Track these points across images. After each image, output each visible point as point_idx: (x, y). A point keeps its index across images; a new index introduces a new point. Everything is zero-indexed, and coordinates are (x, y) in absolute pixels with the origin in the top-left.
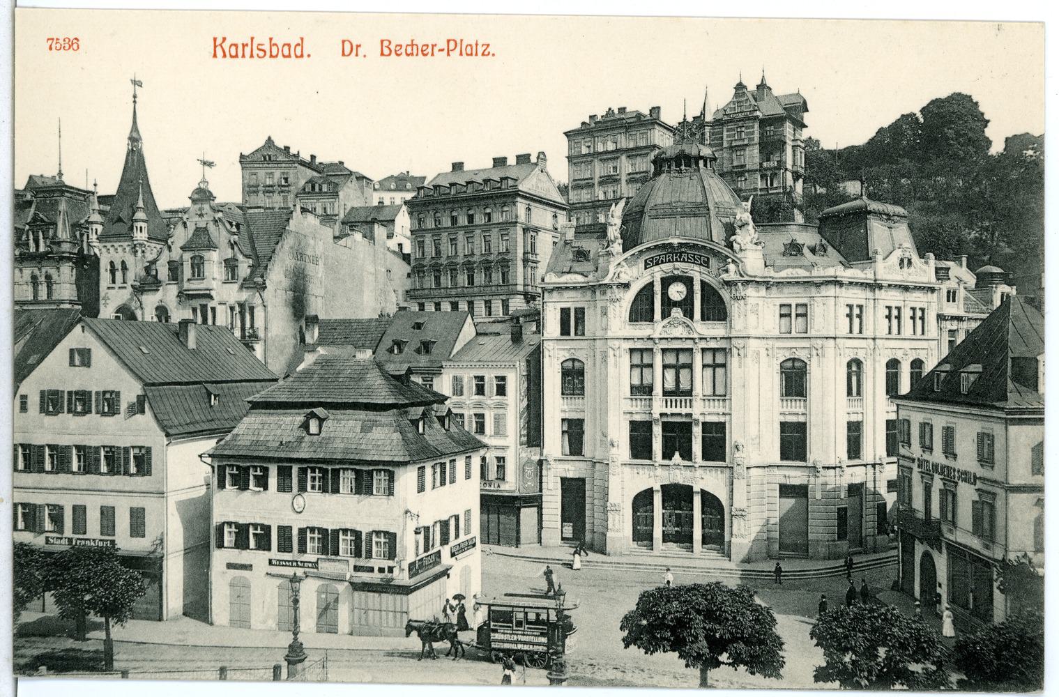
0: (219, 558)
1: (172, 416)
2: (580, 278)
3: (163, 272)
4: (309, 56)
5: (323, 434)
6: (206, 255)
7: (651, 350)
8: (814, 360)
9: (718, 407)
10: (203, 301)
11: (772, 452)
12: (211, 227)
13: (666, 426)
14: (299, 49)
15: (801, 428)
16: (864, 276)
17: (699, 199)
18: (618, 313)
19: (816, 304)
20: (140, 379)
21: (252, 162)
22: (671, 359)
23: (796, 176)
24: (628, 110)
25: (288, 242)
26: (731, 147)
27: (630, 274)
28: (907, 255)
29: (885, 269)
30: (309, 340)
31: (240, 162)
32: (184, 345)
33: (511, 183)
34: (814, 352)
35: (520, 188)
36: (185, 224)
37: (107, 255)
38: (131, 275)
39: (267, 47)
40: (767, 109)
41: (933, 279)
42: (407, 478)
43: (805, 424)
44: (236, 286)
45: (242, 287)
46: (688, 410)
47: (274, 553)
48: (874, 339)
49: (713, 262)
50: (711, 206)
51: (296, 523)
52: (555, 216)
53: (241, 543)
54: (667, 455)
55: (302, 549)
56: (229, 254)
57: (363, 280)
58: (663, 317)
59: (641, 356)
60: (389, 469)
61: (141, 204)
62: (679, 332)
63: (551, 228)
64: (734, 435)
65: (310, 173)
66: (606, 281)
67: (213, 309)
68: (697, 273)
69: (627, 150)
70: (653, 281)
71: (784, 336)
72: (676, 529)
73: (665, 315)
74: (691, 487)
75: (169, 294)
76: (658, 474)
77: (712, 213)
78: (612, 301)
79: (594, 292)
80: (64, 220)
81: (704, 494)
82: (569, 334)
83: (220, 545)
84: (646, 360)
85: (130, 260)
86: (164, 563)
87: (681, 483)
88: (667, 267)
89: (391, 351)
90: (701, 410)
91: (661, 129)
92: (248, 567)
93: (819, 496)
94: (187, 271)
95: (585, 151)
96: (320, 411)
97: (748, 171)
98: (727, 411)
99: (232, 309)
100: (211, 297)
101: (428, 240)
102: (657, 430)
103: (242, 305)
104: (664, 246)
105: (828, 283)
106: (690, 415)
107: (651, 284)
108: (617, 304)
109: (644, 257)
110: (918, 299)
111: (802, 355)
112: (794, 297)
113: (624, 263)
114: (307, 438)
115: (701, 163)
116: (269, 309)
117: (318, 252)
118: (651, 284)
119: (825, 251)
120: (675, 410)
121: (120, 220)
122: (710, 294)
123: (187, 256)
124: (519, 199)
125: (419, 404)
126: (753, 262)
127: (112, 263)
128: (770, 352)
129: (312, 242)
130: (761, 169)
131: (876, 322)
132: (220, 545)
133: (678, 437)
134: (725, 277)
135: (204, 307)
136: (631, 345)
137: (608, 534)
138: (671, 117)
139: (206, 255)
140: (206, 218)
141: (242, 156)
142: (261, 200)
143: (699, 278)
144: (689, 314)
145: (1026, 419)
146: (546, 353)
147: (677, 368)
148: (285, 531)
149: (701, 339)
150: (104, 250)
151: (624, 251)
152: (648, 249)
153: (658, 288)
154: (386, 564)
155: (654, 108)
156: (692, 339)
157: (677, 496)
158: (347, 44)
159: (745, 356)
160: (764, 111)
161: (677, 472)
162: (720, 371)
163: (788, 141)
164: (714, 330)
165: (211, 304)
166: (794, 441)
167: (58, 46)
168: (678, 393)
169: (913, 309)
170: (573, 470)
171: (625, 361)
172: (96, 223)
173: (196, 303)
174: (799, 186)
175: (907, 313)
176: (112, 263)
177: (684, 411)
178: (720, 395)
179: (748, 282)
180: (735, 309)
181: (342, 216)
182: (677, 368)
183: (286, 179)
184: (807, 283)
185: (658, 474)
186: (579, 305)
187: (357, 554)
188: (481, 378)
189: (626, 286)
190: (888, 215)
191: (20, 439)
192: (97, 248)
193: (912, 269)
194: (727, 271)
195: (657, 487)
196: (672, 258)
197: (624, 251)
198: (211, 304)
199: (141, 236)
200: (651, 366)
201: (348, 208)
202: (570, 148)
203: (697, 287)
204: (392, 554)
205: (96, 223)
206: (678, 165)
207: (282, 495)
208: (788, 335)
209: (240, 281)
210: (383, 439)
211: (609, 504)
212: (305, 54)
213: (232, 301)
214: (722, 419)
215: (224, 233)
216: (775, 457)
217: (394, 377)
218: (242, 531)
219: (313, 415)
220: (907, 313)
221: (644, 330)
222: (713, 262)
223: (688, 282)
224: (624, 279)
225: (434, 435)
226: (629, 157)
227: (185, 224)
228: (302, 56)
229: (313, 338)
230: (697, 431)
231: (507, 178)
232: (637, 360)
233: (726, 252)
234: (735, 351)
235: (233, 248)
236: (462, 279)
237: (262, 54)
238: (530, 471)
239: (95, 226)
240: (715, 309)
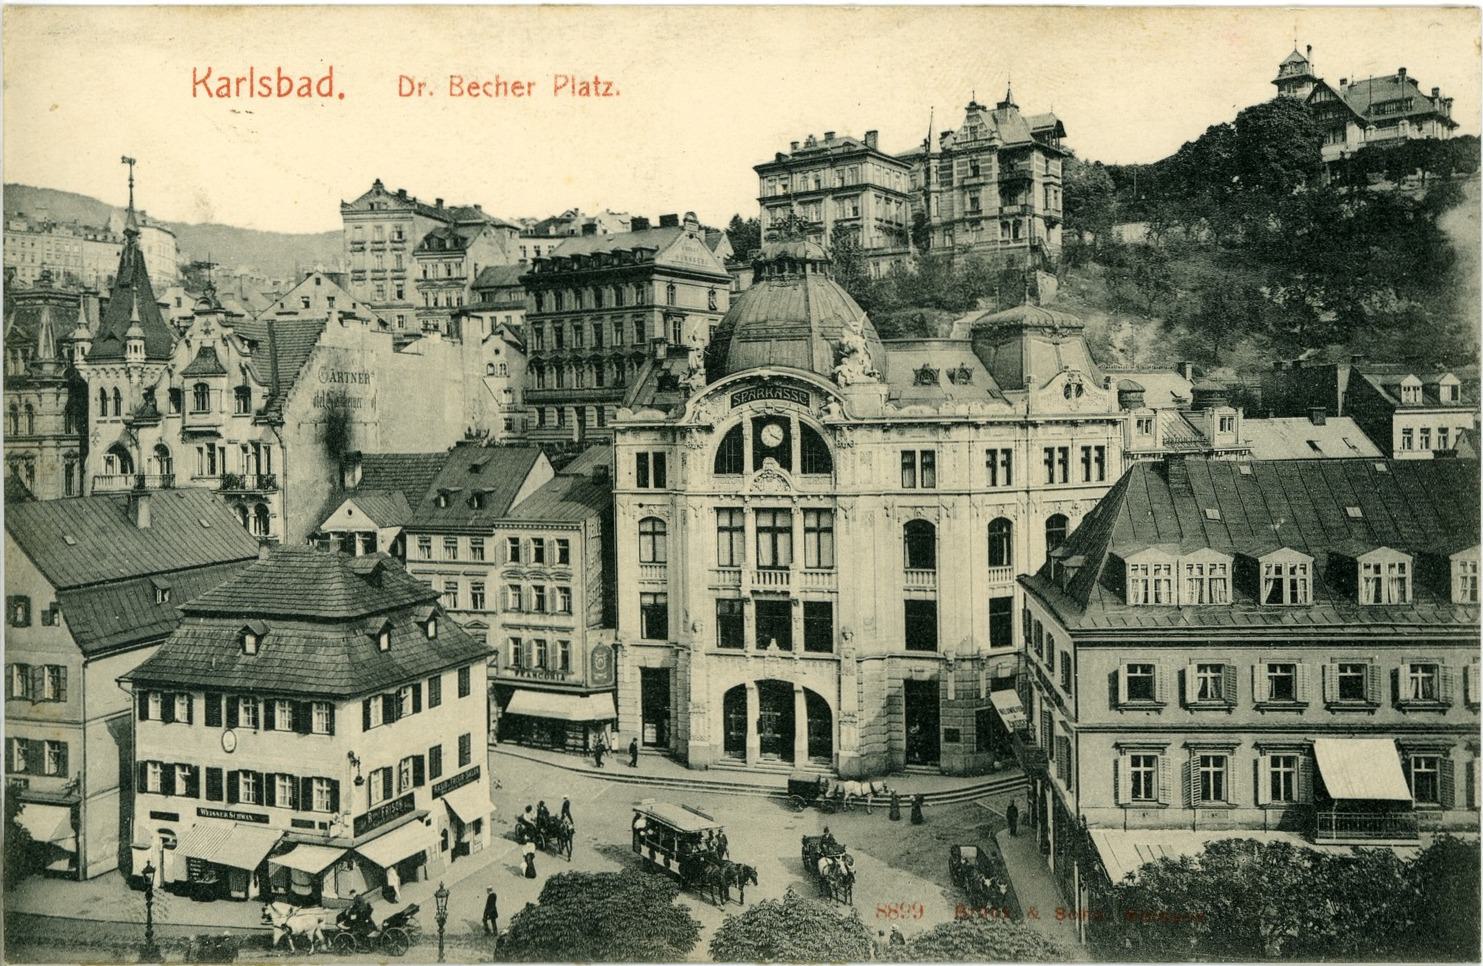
0: (143, 804)
1: (95, 624)
2: (661, 415)
3: (163, 401)
4: (341, 96)
5: (261, 654)
6: (212, 382)
7: (741, 509)
8: (944, 521)
9: (824, 583)
10: (210, 440)
12: (220, 348)
14: (326, 83)
16: (1012, 412)
17: (802, 316)
20: (53, 583)
21: (357, 212)
22: (766, 521)
23: (1050, 223)
24: (837, 136)
25: (320, 361)
26: (963, 187)
27: (712, 411)
28: (1076, 380)
29: (1047, 401)
30: (349, 483)
31: (343, 213)
32: (133, 524)
33: (646, 255)
34: (943, 512)
35: (658, 261)
36: (187, 342)
37: (97, 379)
38: (125, 408)
39: (273, 84)
40: (1012, 134)
41: (1116, 406)
42: (349, 714)
44: (249, 421)
45: (255, 424)
46: (784, 587)
47: (203, 802)
48: (1028, 492)
49: (814, 400)
50: (814, 324)
51: (227, 765)
52: (712, 293)
53: (168, 788)
54: (763, 644)
55: (234, 798)
56: (239, 382)
57: (443, 391)
58: (755, 469)
59: (730, 519)
60: (331, 701)
61: (135, 317)
62: (773, 486)
63: (706, 308)
64: (841, 619)
65: (431, 224)
66: (683, 423)
67: (222, 450)
68: (794, 412)
69: (833, 191)
71: (906, 491)
73: (757, 465)
74: (792, 685)
75: (169, 430)
76: (753, 667)
77: (816, 335)
78: (691, 447)
80: (47, 336)
81: (808, 693)
82: (647, 486)
83: (143, 789)
84: (737, 522)
85: (123, 383)
86: (82, 808)
88: (758, 404)
89: (437, 502)
90: (800, 587)
91: (876, 161)
92: (174, 817)
93: (951, 696)
94: (189, 400)
95: (780, 191)
96: (254, 624)
97: (986, 218)
98: (833, 587)
99: (245, 449)
100: (219, 435)
101: (548, 325)
102: (750, 611)
103: (256, 445)
104: (752, 380)
105: (958, 424)
106: (786, 593)
108: (698, 451)
110: (1094, 436)
111: (929, 516)
112: (918, 441)
113: (703, 400)
114: (244, 659)
115: (809, 267)
116: (289, 450)
117: (368, 367)
119: (969, 377)
120: (769, 587)
121: (112, 337)
123: (190, 383)
124: (656, 276)
125: (378, 614)
126: (866, 398)
127: (103, 391)
128: (890, 512)
129: (357, 356)
130: (1002, 216)
131: (1029, 467)
132: (143, 789)
133: (774, 620)
134: (827, 419)
135: (212, 447)
136: (717, 503)
137: (691, 743)
138: (888, 146)
139: (212, 382)
140: (213, 335)
141: (344, 205)
144: (786, 464)
146: (620, 510)
147: (774, 531)
148: (214, 774)
150: (93, 373)
151: (709, 382)
152: (734, 383)
154: (327, 817)
155: (869, 133)
156: (790, 497)
157: (777, 694)
158: (405, 83)
159: (854, 519)
160: (1004, 137)
161: (773, 665)
162: (825, 538)
163: (1035, 178)
164: (819, 484)
165: (219, 443)
166: (921, 624)
168: (776, 567)
169: (1086, 449)
170: (656, 658)
171: (710, 522)
172: (83, 340)
173: (203, 443)
174: (1057, 233)
175: (1075, 456)
176: (103, 391)
177: (780, 588)
178: (825, 567)
179: (856, 426)
180: (841, 458)
181: (471, 279)
182: (774, 531)
183: (400, 234)
184: (935, 426)
185: (753, 667)
186: (658, 449)
187: (294, 805)
188: (539, 541)
189: (709, 429)
190: (1052, 327)
192: (84, 370)
193: (1084, 396)
194: (828, 411)
197: (709, 382)
198: (219, 443)
199: (136, 357)
200: (742, 529)
201: (480, 269)
202: (762, 188)
203: (796, 431)
204: (334, 806)
205: (83, 340)
206: (781, 270)
207: (210, 729)
208: (912, 491)
209: (253, 414)
210: (328, 658)
211: (691, 706)
212: (336, 93)
213: (244, 440)
214: (827, 598)
215: (234, 354)
216: (900, 646)
217: (363, 576)
218: (168, 771)
219: (247, 630)
220: (1075, 456)
221: (730, 483)
222: (814, 400)
223: (784, 423)
224: (705, 421)
225: (407, 646)
226: (835, 199)
227: (187, 342)
228: (330, 94)
229: (353, 479)
230: (798, 613)
231: (641, 249)
232: (725, 521)
233: (827, 386)
234: (840, 513)
235: (245, 374)
236: (590, 379)
237: (265, 91)
238: (601, 659)
239: (81, 344)
240: (818, 460)
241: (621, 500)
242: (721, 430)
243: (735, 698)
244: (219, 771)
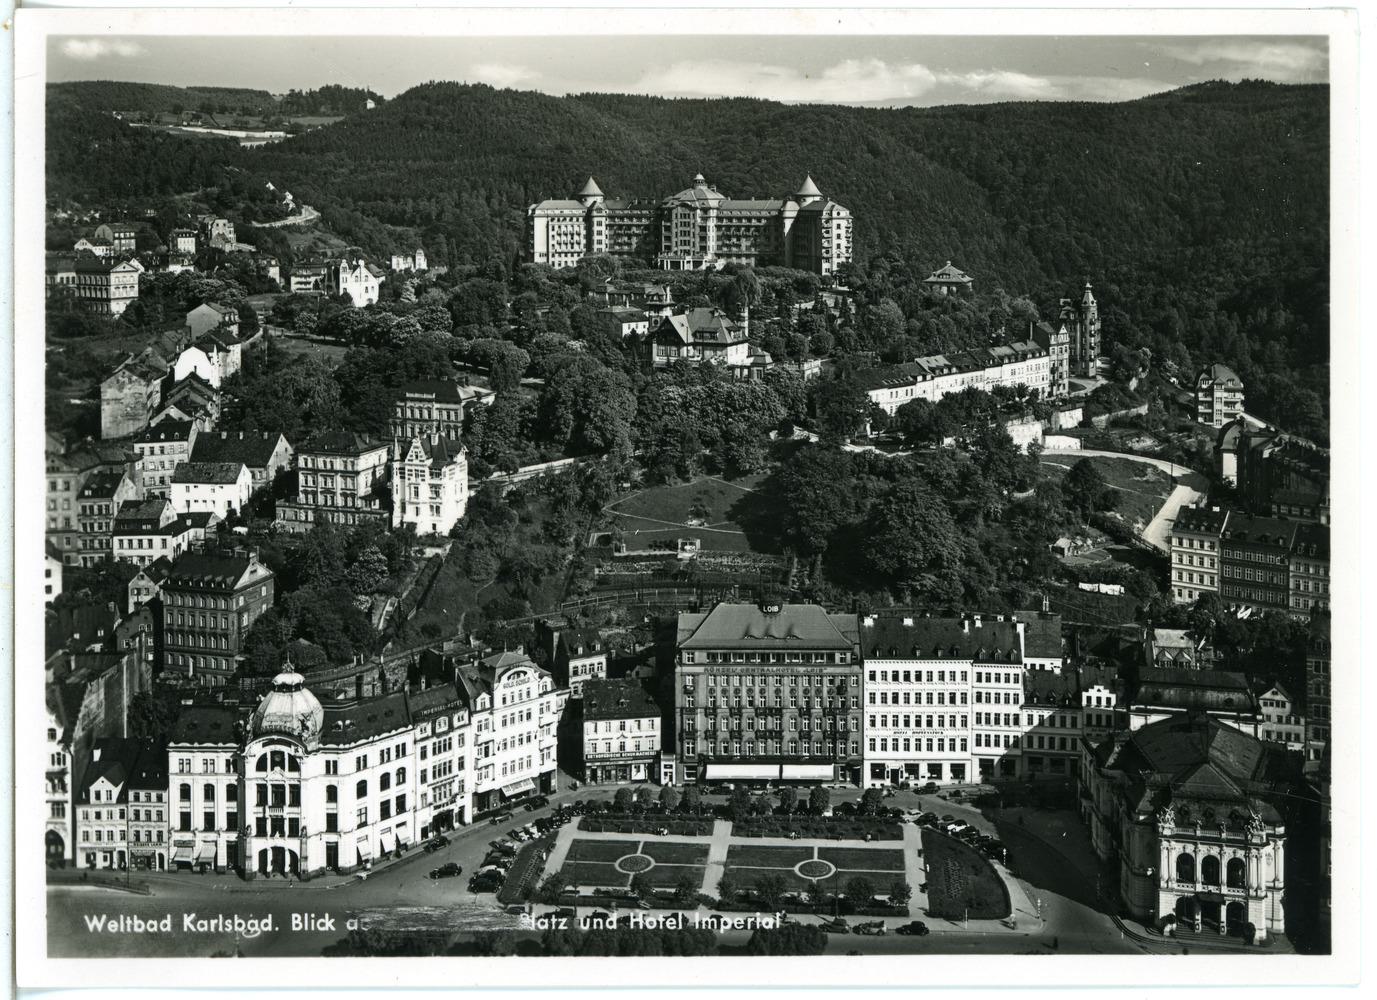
11: (324, 827)
15: (335, 815)
62: (279, 777)
76: (268, 843)
81: (291, 852)
102: (269, 822)
111: (334, 783)
122: (292, 759)
142: (338, 464)
144: (283, 768)
145: (660, 548)
157: (279, 852)
161: (278, 842)
164: (295, 775)
167: (576, 238)
180: (303, 767)
182: (726, 658)
185: (268, 843)
191: (696, 328)
221: (262, 774)
230: (287, 823)
240: (295, 766)
241: (171, 777)
243: (263, 854)
244: (282, 787)
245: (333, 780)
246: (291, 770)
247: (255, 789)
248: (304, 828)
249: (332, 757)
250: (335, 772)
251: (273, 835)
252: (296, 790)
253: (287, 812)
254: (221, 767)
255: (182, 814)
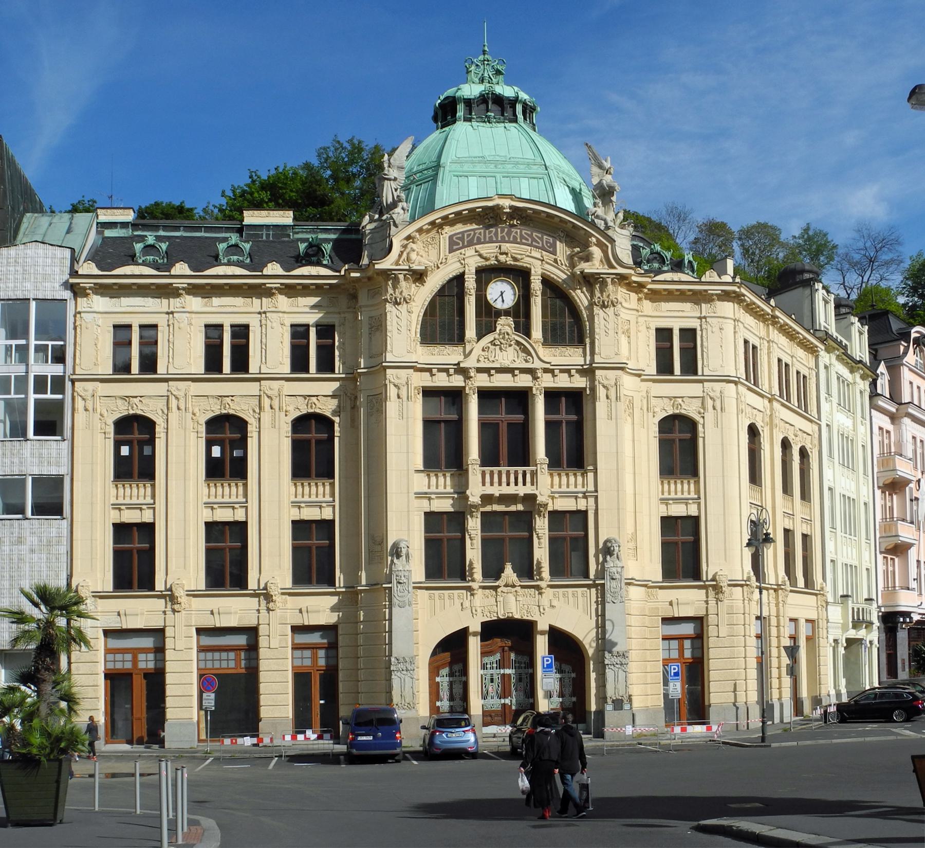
8: (710, 415)
13: (488, 520)
15: (693, 524)
18: (404, 323)
19: (709, 329)
43: (696, 520)
54: (492, 571)
58: (480, 336)
62: (509, 357)
70: (463, 274)
72: (503, 701)
73: (484, 329)
76: (467, 608)
79: (354, 297)
87: (517, 616)
106: (533, 497)
107: (460, 279)
108: (403, 308)
109: (448, 231)
111: (690, 410)
118: (460, 279)
134: (588, 268)
136: (425, 380)
143: (540, 272)
144: (524, 328)
149: (546, 371)
153: (470, 283)
157: (511, 635)
189: (419, 276)
195: (476, 627)
196: (496, 234)
203: (536, 285)
214: (582, 505)
221: (450, 355)
240: (568, 326)
242: (434, 282)
245: (682, 395)
246: (554, 337)
247: (417, 409)
248: (607, 550)
249: (679, 315)
250: (690, 366)
251: (492, 571)
252: (572, 406)
253: (551, 488)
254: (271, 350)
255: (121, 530)
